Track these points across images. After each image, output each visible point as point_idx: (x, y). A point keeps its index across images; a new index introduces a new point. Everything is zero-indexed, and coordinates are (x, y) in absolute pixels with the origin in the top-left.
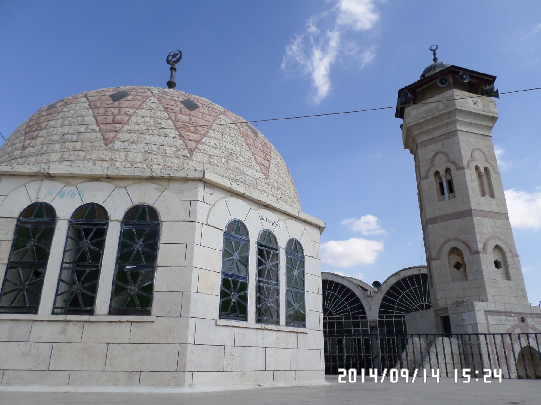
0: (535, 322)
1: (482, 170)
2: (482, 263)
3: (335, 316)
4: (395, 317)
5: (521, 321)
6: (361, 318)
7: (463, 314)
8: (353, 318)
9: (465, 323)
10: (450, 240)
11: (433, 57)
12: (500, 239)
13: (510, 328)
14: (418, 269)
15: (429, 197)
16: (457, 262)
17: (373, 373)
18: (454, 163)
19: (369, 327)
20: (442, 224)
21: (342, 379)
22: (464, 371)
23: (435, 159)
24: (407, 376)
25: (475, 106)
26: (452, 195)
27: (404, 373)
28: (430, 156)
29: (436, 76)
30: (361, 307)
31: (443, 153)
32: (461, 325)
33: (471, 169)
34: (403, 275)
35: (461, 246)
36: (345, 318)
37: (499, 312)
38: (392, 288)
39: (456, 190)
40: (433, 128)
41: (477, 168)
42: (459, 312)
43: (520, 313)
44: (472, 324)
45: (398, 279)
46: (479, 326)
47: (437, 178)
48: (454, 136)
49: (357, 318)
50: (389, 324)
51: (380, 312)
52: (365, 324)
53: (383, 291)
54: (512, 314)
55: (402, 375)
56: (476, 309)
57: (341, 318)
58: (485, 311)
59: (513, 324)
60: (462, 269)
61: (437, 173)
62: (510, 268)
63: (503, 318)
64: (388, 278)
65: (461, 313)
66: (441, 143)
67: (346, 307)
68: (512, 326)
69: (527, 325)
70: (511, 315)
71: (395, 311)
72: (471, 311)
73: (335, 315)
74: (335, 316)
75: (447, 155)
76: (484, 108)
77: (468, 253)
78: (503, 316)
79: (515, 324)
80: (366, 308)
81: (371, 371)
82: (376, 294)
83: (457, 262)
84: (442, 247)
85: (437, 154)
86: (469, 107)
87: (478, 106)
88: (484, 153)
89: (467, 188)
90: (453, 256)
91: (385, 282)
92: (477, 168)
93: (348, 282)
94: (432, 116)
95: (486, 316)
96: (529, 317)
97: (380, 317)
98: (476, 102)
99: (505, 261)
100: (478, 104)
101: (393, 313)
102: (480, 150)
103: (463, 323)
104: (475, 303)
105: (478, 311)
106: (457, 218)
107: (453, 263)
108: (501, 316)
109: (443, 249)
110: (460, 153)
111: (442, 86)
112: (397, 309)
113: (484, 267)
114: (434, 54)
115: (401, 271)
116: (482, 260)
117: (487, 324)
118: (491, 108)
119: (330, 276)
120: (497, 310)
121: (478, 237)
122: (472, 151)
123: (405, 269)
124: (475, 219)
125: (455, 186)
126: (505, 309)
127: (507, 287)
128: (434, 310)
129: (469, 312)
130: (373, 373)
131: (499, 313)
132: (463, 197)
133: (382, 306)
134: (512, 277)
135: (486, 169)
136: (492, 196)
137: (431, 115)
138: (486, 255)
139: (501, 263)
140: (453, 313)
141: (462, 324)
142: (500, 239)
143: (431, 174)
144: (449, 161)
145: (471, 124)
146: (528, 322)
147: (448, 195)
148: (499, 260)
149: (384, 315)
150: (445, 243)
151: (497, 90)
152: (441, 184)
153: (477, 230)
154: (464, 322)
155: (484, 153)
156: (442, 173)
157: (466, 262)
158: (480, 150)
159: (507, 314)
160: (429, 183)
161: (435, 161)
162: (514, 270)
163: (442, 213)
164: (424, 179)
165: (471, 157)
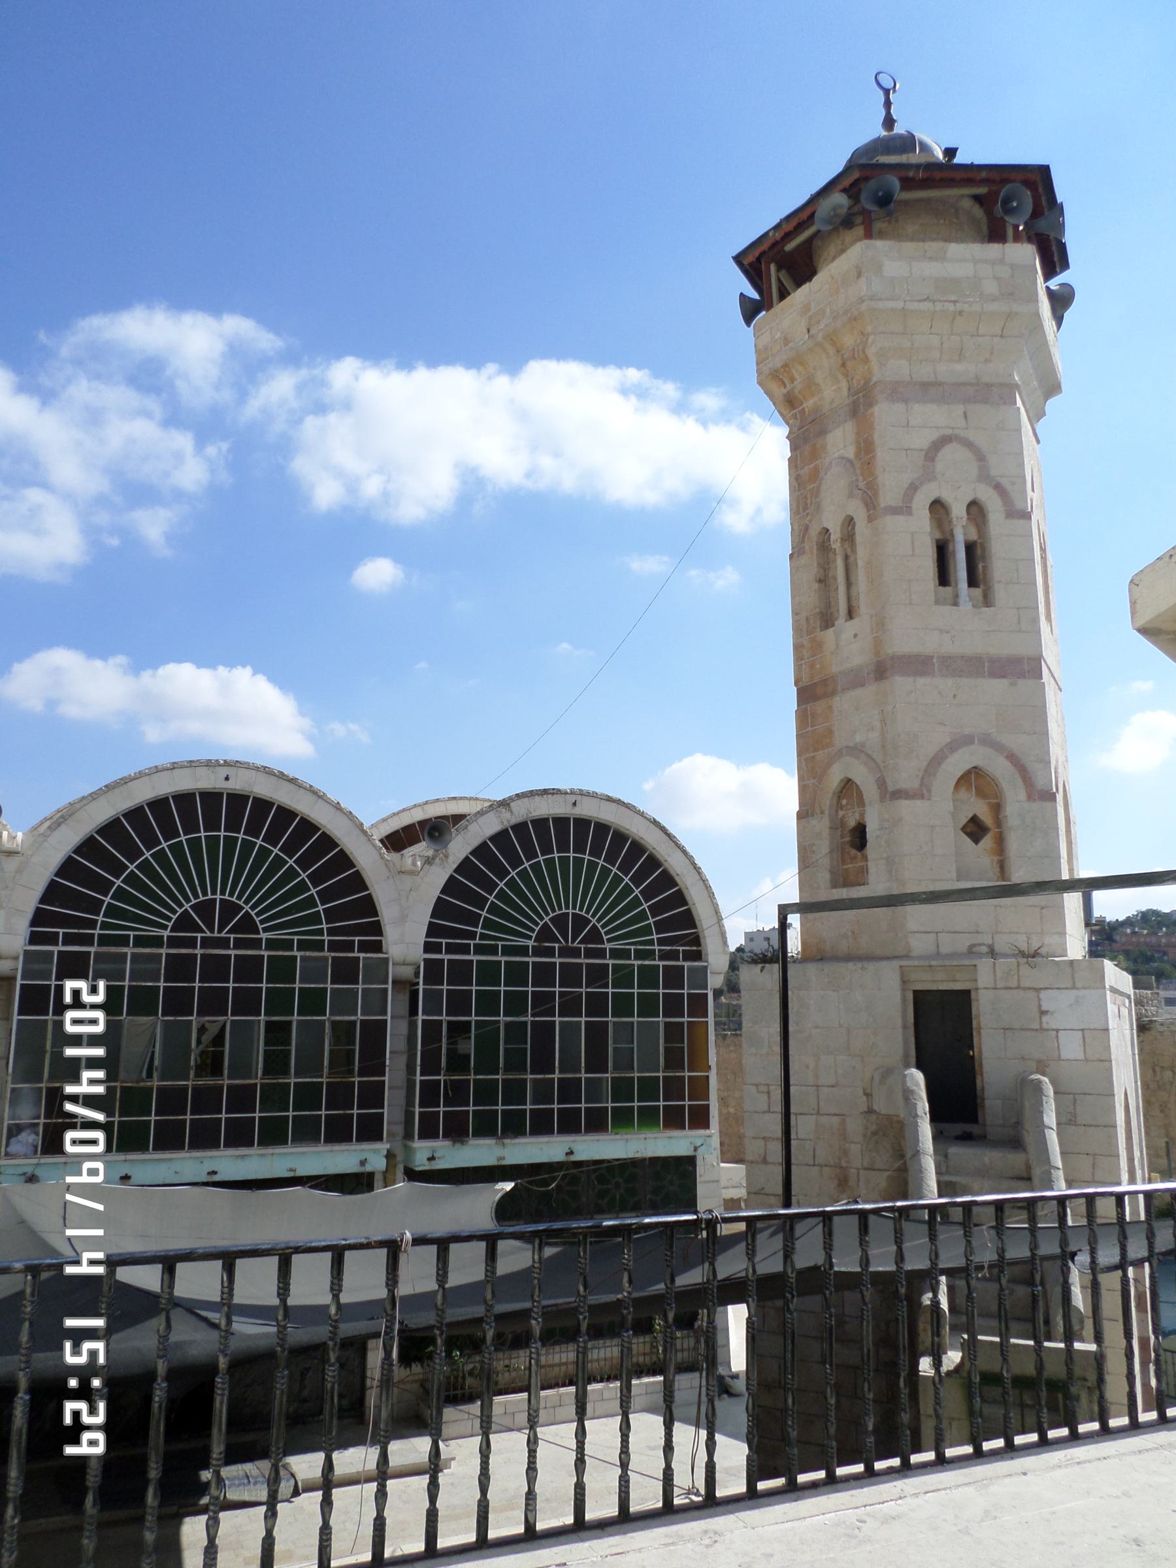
3: (264, 936)
4: (480, 950)
6: (364, 946)
8: (334, 946)
9: (1049, 1022)
10: (968, 740)
11: (883, 113)
14: (572, 798)
17: (92, 1082)
18: (999, 488)
21: (76, 993)
22: (99, 1346)
23: (940, 456)
24: (85, 1179)
26: (977, 592)
27: (93, 1172)
28: (922, 440)
30: (368, 906)
31: (968, 444)
35: (1000, 768)
36: (303, 946)
44: (1083, 1030)
45: (506, 823)
48: (1005, 403)
49: (349, 946)
50: (460, 972)
51: (433, 930)
53: (451, 858)
55: (87, 1165)
57: (288, 945)
60: (987, 842)
61: (938, 507)
67: (310, 903)
71: (479, 930)
72: (1084, 988)
73: (265, 930)
74: (264, 936)
77: (1022, 795)
80: (387, 913)
81: (100, 1074)
82: (426, 866)
84: (937, 760)
90: (963, 794)
93: (334, 810)
94: (959, 306)
101: (472, 935)
103: (1041, 1023)
106: (993, 674)
109: (944, 766)
112: (488, 924)
114: (888, 104)
119: (262, 777)
123: (532, 794)
125: (999, 567)
128: (901, 967)
129: (1074, 987)
130: (92, 1082)
132: (1018, 609)
133: (440, 909)
137: (955, 302)
140: (1000, 984)
141: (1036, 1026)
143: (922, 503)
144: (984, 476)
154: (1045, 1019)
160: (913, 534)
161: (939, 465)
164: (898, 514)
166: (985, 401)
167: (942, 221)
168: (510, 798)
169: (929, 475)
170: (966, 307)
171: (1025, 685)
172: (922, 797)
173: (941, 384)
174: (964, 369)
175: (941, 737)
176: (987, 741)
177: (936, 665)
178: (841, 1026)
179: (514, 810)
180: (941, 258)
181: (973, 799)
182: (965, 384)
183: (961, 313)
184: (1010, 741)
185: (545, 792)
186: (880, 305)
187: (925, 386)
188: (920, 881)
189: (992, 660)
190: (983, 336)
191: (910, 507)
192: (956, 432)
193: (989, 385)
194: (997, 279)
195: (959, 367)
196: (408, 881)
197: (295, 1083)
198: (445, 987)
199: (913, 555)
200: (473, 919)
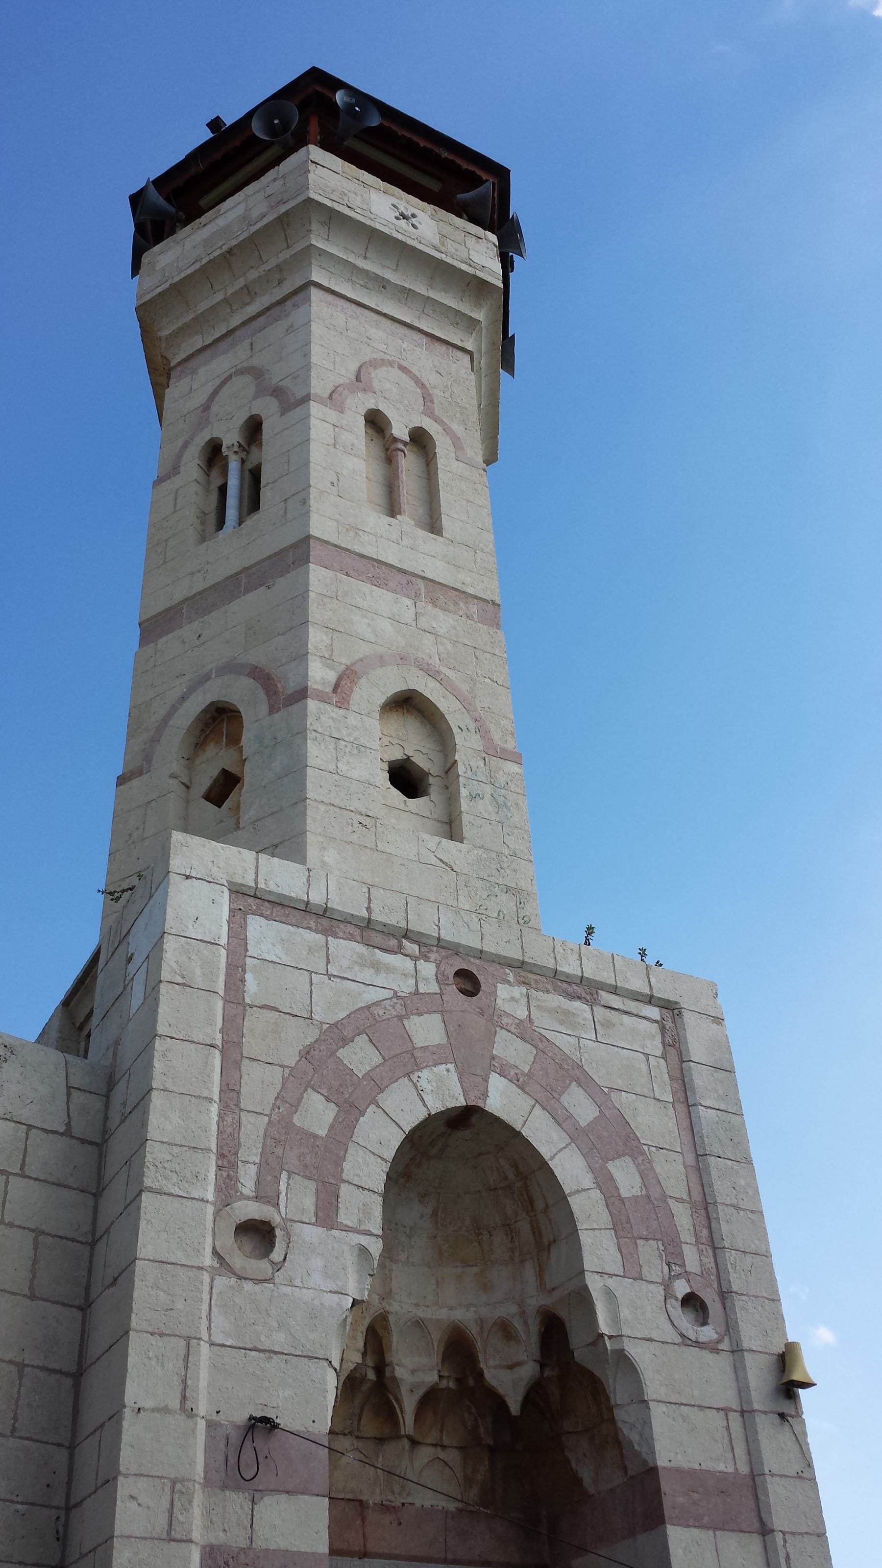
0: (539, 1007)
2: (311, 735)
5: (463, 991)
13: (377, 1004)
16: (224, 771)
18: (277, 392)
33: (342, 412)
40: (225, 300)
43: (454, 949)
58: (237, 891)
59: (406, 987)
62: (464, 792)
68: (396, 995)
70: (400, 946)
77: (263, 708)
78: (350, 937)
79: (417, 992)
83: (224, 771)
86: (372, 216)
88: (423, 386)
96: (511, 978)
99: (450, 769)
104: (177, 837)
108: (335, 936)
117: (229, 948)
120: (317, 898)
121: (316, 638)
126: (368, 909)
127: (434, 861)
131: (325, 922)
136: (433, 525)
138: (342, 712)
139: (427, 774)
145: (383, 284)
146: (499, 1001)
148: (420, 761)
159: (378, 939)
162: (484, 807)
165: (354, 378)
177: (185, 614)
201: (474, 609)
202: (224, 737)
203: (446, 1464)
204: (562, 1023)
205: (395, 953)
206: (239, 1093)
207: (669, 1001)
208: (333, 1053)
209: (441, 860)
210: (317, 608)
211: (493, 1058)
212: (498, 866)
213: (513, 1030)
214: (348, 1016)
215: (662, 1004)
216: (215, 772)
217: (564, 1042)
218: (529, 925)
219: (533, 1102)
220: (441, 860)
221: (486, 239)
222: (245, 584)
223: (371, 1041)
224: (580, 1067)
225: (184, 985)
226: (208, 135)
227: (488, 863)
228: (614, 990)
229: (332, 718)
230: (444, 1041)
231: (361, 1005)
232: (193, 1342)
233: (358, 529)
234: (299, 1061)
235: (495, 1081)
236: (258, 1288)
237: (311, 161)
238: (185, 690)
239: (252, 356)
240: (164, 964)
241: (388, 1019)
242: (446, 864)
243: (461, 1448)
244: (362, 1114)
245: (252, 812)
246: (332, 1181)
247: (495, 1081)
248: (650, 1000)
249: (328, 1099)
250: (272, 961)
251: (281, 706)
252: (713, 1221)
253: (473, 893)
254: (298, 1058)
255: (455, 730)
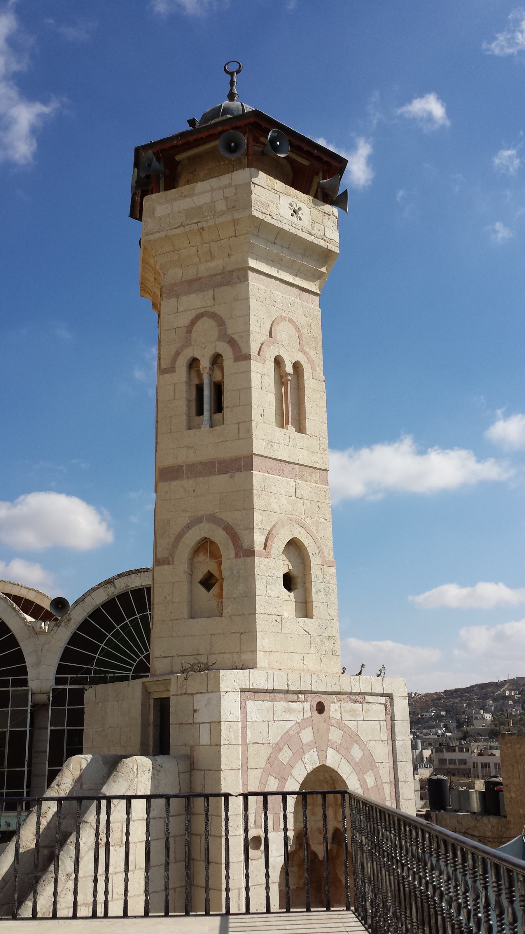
0: (344, 711)
1: (289, 369)
2: (257, 577)
6: (16, 683)
7: (196, 697)
12: (302, 526)
15: (171, 417)
19: (30, 704)
20: (188, 483)
23: (195, 328)
25: (295, 218)
26: (218, 416)
28: (184, 320)
29: (220, 129)
31: (214, 316)
32: (190, 724)
34: (121, 586)
37: (273, 691)
38: (96, 614)
39: (228, 407)
41: (278, 362)
42: (189, 691)
44: (210, 723)
45: (110, 594)
46: (223, 726)
47: (194, 374)
48: (241, 282)
51: (61, 669)
52: (22, 699)
53: (73, 621)
54: (299, 695)
56: (223, 687)
60: (215, 590)
61: (193, 363)
62: (314, 590)
63: (280, 705)
64: (89, 591)
65: (193, 694)
66: (210, 293)
69: (328, 721)
71: (94, 667)
72: (212, 692)
75: (221, 322)
76: (313, 227)
77: (232, 554)
80: (29, 660)
82: (55, 628)
85: (199, 317)
86: (281, 218)
87: (300, 219)
89: (249, 404)
91: (80, 601)
92: (278, 362)
95: (243, 702)
97: (58, 681)
98: (296, 208)
100: (301, 216)
102: (290, 320)
105: (227, 692)
106: (221, 472)
107: (200, 575)
109: (183, 540)
110: (248, 323)
111: (227, 155)
113: (260, 587)
115: (120, 576)
116: (257, 571)
118: (326, 229)
120: (270, 687)
121: (257, 517)
122: (273, 322)
123: (129, 573)
124: (257, 476)
125: (227, 399)
129: (208, 692)
132: (238, 423)
133: (67, 655)
134: (315, 611)
135: (297, 366)
137: (197, 223)
138: (268, 560)
140: (179, 693)
141: (191, 722)
142: (302, 526)
147: (211, 417)
148: (295, 573)
149: (69, 676)
150: (189, 527)
151: (346, 192)
152: (200, 389)
153: (257, 503)
155: (298, 329)
156: (205, 364)
157: (225, 574)
158: (290, 320)
161: (194, 335)
163: (192, 458)
166: (228, 283)
167: (222, 163)
168: (114, 578)
169: (188, 343)
170: (205, 225)
171: (240, 476)
172: (169, 564)
173: (200, 278)
174: (216, 265)
175: (183, 520)
176: (213, 519)
177: (185, 471)
178: (118, 726)
179: (117, 586)
180: (192, 195)
181: (207, 561)
182: (215, 275)
183: (203, 229)
184: (228, 517)
185: (138, 571)
186: (152, 237)
187: (190, 282)
188: (164, 621)
189: (221, 462)
190: (223, 239)
191: (175, 367)
192: (207, 309)
193: (231, 272)
194: (225, 198)
195: (212, 264)
196: (42, 638)
197: (7, 771)
198: (67, 707)
199: (174, 399)
200: (89, 660)
201: (318, 475)
202: (208, 552)
203: (293, 872)
204: (352, 716)
205: (296, 702)
206: (247, 785)
207: (389, 694)
208: (276, 757)
209: (305, 630)
210: (257, 499)
211: (329, 741)
212: (326, 626)
213: (335, 725)
214: (281, 738)
215: (387, 695)
216: (205, 571)
217: (352, 725)
218: (336, 654)
219: (341, 756)
220: (305, 630)
221: (333, 215)
222: (217, 467)
223: (289, 747)
224: (357, 735)
225: (229, 744)
226: (187, 128)
227: (322, 626)
228: (371, 694)
229: (265, 565)
230: (313, 739)
231: (285, 731)
232: (240, 890)
233: (272, 442)
234: (266, 764)
235: (330, 751)
236: (257, 862)
237: (253, 183)
238: (188, 521)
239: (214, 305)
240: (222, 737)
241: (294, 735)
242: (307, 632)
243: (298, 865)
244: (286, 780)
245: (229, 610)
246: (278, 812)
247: (330, 751)
248: (382, 695)
249: (276, 778)
250: (256, 721)
251: (241, 555)
252: (397, 789)
253: (316, 644)
254: (265, 763)
255: (311, 555)
